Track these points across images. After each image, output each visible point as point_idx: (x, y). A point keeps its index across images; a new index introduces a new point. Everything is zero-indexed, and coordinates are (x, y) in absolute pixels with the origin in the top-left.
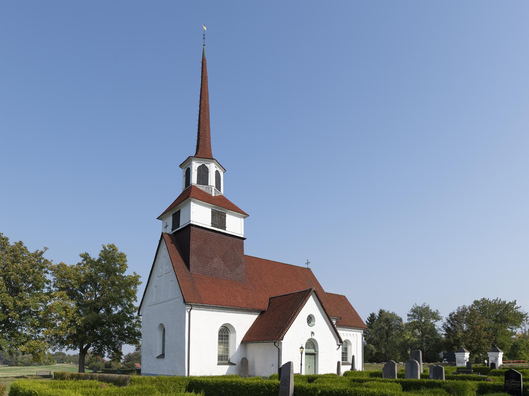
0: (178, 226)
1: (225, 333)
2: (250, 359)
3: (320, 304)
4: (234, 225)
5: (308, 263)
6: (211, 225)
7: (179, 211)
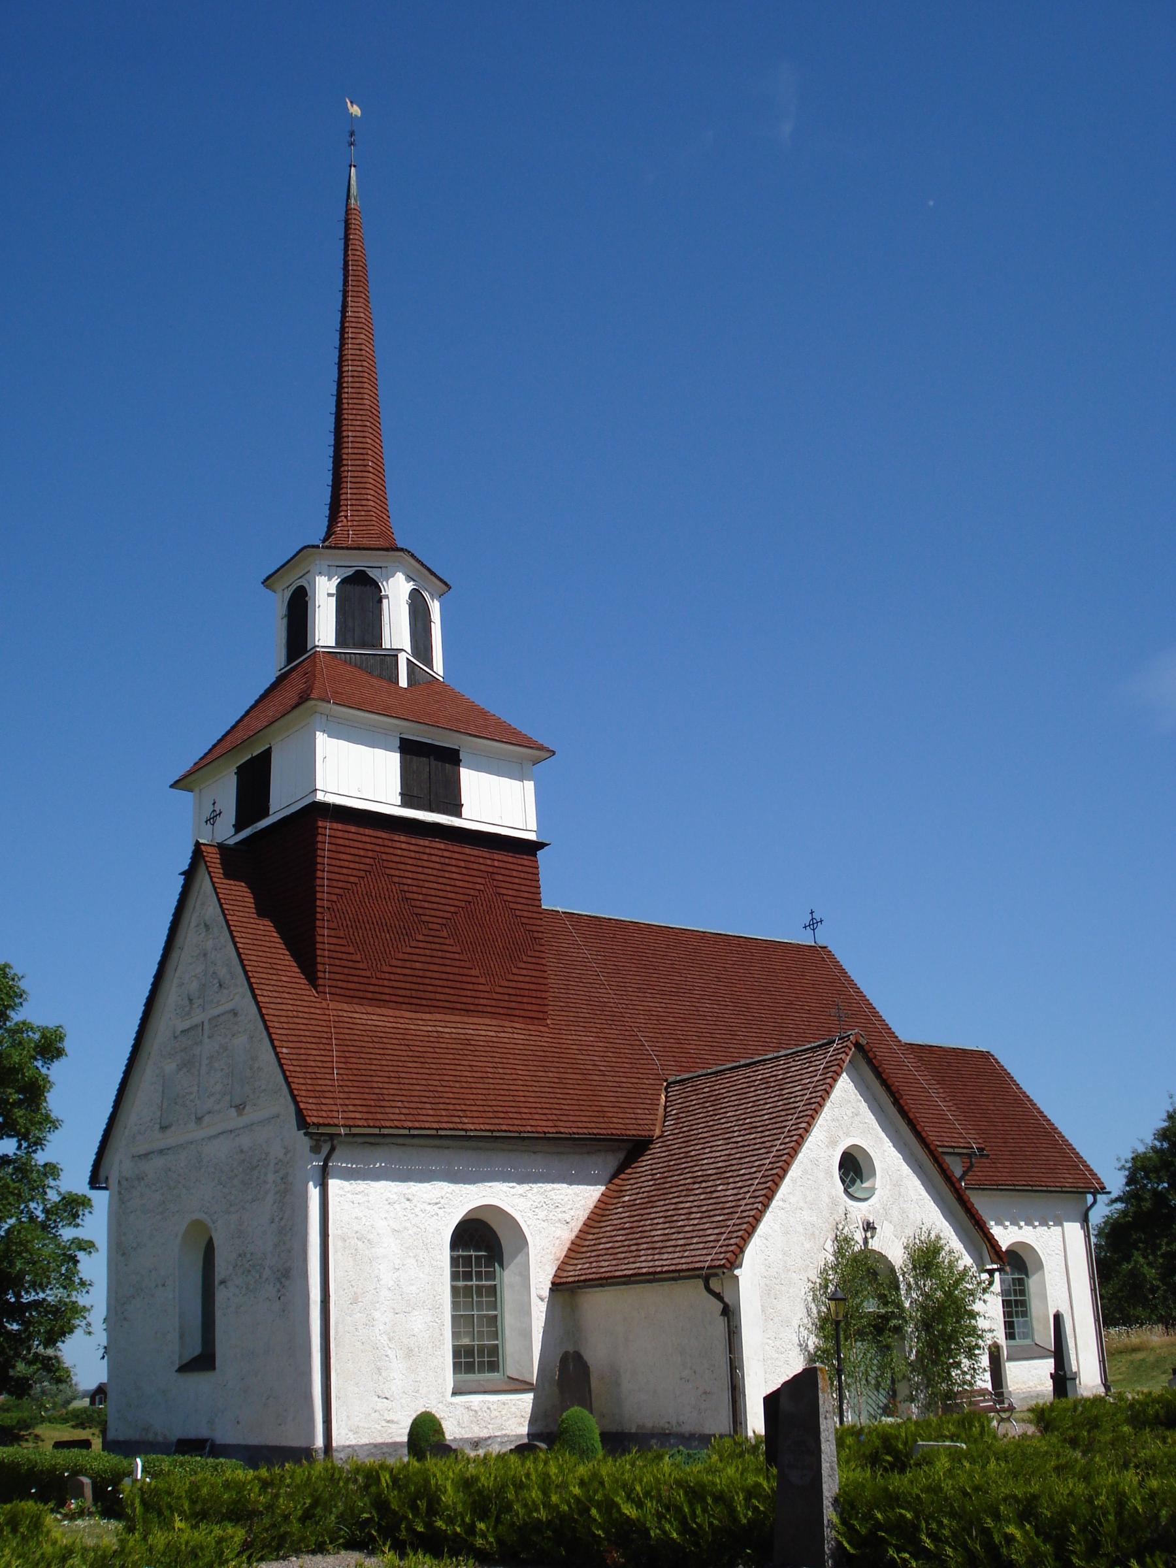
0: (241, 771)
1: (481, 1245)
2: (596, 1354)
3: (892, 1110)
4: (495, 801)
5: (813, 924)
6: (398, 800)
7: (266, 756)
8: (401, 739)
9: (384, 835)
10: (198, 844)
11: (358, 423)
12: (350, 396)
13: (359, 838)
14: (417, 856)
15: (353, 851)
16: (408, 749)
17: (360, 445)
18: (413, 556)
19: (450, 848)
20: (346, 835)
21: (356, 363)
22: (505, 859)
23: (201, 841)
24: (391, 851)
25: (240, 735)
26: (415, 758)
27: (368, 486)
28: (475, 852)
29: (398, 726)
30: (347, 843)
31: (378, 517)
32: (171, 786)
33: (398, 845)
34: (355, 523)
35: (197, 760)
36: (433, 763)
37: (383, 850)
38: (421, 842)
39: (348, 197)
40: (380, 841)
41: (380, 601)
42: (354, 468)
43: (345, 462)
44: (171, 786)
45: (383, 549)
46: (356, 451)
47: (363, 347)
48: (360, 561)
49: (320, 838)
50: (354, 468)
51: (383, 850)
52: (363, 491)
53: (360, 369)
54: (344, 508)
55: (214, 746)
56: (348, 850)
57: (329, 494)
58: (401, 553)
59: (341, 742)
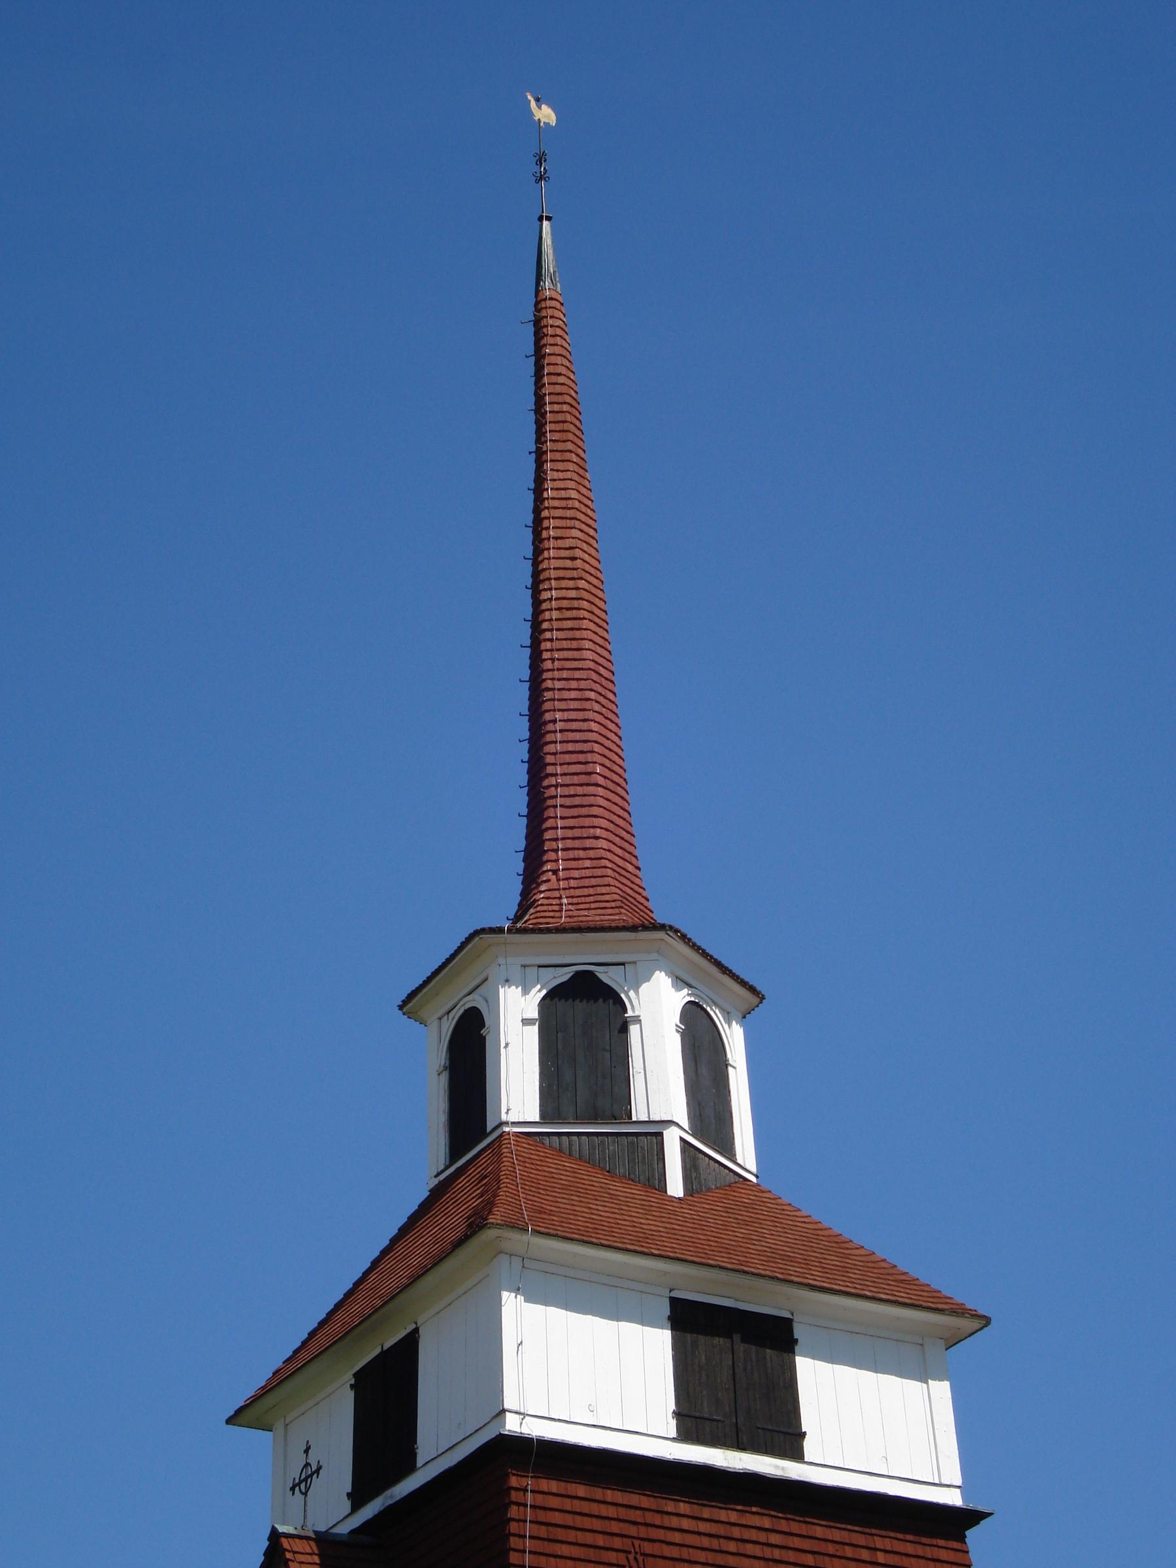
0: (363, 1382)
4: (872, 1426)
7: (409, 1347)
8: (671, 1298)
9: (645, 1502)
10: (275, 1536)
11: (573, 695)
12: (557, 645)
13: (595, 1508)
14: (715, 1544)
15: (582, 1537)
16: (687, 1319)
17: (578, 736)
18: (684, 937)
19: (783, 1525)
20: (568, 1504)
21: (564, 583)
22: (899, 1546)
23: (282, 1529)
24: (661, 1534)
25: (357, 1308)
26: (702, 1339)
27: (596, 811)
28: (837, 1535)
29: (665, 1273)
30: (569, 1520)
31: (619, 871)
32: (229, 1421)
33: (674, 1522)
34: (574, 890)
35: (278, 1364)
36: (741, 1348)
37: (643, 1532)
38: (723, 1515)
39: (539, 277)
40: (636, 1515)
41: (624, 1029)
42: (567, 780)
43: (550, 770)
44: (229, 1421)
45: (625, 929)
46: (570, 747)
47: (578, 553)
48: (581, 954)
49: (513, 1512)
50: (567, 780)
51: (643, 1532)
52: (587, 822)
53: (573, 594)
54: (552, 856)
55: (312, 1334)
56: (572, 1536)
57: (523, 832)
58: (661, 935)
59: (552, 1310)
